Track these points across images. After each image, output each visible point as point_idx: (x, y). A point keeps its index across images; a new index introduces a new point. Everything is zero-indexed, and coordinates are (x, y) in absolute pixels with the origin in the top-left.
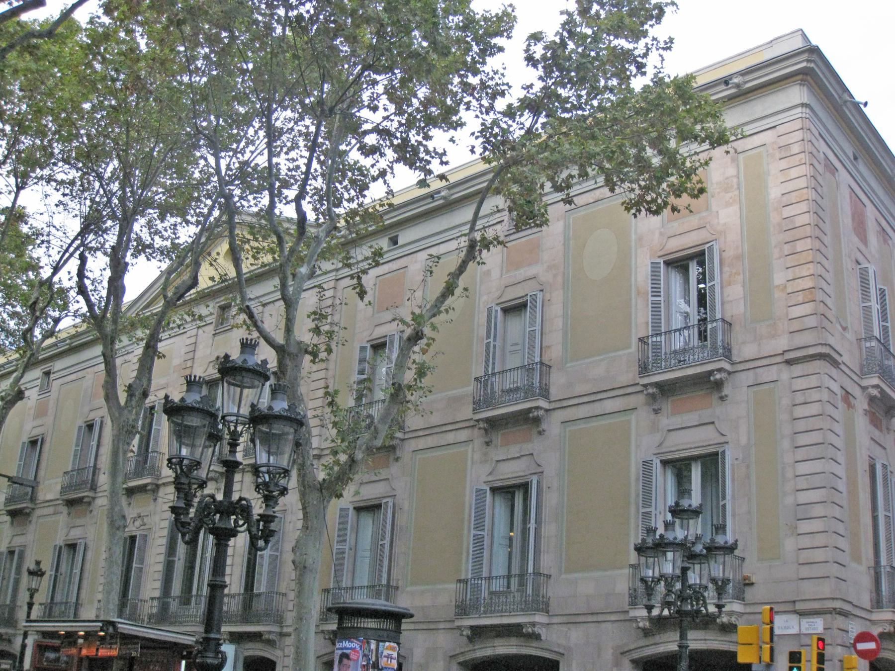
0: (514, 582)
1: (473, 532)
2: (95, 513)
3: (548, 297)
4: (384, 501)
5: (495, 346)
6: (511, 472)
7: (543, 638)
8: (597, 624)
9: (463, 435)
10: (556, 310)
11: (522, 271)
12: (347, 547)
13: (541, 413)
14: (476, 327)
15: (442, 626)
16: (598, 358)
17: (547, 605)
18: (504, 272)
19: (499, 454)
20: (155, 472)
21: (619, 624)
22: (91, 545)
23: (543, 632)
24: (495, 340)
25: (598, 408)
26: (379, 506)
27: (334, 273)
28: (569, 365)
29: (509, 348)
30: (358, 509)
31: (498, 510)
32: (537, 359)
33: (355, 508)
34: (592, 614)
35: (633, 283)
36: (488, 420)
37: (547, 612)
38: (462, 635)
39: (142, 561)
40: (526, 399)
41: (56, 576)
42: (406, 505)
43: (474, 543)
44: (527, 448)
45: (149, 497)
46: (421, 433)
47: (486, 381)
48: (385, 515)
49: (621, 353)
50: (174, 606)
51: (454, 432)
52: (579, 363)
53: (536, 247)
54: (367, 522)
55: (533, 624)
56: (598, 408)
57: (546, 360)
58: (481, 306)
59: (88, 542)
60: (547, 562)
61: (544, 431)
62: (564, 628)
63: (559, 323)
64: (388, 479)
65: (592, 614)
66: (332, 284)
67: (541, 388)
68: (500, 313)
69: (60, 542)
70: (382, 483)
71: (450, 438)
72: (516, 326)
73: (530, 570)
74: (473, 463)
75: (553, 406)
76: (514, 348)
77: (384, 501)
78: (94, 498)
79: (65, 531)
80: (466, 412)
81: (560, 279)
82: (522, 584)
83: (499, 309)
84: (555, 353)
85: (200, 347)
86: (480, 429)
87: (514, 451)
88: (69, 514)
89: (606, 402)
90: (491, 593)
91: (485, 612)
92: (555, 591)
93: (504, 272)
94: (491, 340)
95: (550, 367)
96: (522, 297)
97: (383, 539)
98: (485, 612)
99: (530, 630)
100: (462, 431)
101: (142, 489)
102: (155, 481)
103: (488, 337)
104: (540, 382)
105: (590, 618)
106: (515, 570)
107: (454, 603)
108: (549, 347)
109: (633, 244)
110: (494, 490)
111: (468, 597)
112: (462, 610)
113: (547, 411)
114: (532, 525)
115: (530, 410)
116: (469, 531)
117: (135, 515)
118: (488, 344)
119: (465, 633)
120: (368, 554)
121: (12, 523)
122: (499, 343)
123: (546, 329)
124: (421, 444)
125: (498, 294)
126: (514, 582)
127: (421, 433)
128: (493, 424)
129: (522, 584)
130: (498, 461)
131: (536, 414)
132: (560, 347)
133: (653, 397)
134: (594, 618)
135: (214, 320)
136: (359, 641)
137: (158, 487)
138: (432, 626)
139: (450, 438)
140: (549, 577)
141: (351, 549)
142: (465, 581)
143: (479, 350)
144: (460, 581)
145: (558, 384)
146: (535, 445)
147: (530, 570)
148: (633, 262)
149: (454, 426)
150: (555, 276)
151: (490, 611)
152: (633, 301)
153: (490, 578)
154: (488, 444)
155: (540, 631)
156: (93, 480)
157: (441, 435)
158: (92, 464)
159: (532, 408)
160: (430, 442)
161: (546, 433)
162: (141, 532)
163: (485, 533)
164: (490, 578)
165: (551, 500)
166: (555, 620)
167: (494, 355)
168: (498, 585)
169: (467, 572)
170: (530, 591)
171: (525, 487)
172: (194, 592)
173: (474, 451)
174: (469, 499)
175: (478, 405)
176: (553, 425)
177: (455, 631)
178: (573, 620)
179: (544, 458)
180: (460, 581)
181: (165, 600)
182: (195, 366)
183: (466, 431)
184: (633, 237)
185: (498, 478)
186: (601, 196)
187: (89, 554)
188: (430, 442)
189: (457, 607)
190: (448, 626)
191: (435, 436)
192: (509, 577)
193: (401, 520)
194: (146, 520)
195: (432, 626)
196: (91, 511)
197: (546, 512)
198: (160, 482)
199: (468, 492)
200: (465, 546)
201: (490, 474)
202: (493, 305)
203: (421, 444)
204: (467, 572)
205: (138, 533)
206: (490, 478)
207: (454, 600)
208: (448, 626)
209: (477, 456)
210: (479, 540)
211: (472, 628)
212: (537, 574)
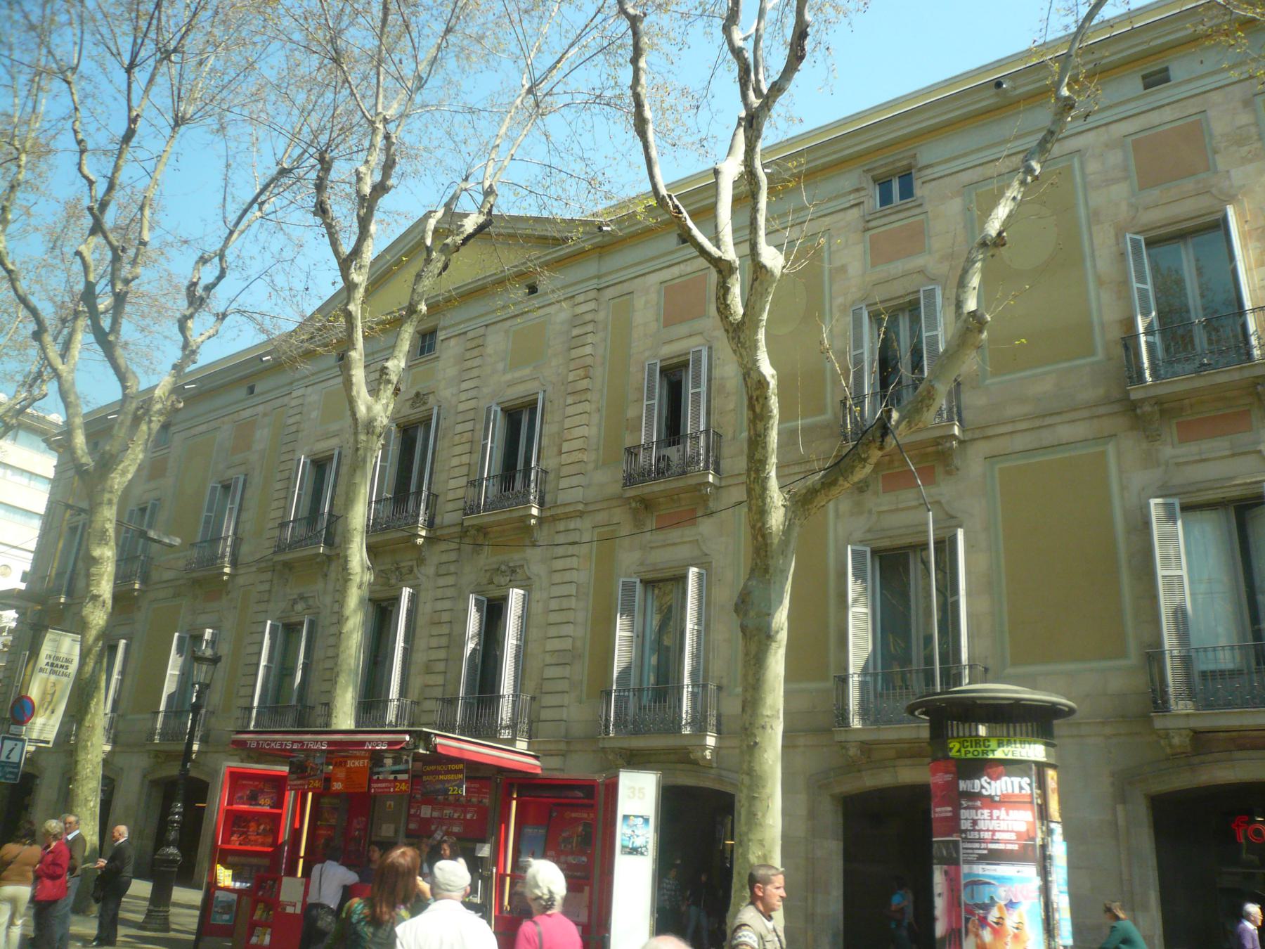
28: (988, 382)
66: (593, 294)
110: (648, 584)
176: (974, 464)
184: (1082, 212)
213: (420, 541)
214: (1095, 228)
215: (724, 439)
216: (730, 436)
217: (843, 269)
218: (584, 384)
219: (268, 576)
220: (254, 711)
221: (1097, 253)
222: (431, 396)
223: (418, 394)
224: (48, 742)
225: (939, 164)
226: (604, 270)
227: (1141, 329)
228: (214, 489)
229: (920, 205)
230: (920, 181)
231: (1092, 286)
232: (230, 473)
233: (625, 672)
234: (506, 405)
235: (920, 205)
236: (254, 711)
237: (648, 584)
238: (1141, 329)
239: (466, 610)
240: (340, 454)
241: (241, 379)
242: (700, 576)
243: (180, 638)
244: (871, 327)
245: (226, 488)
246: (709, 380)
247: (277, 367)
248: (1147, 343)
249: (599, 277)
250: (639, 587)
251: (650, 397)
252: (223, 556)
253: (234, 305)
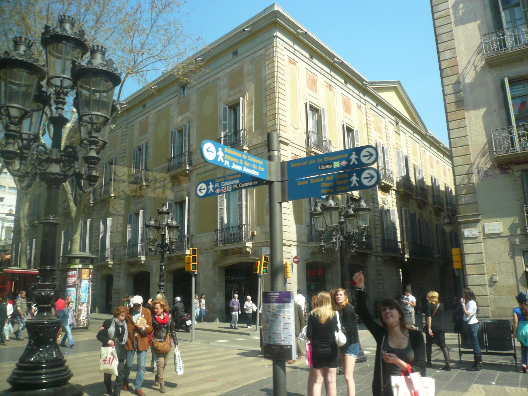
21: (306, 248)
66: (125, 126)
208: (212, 251)
213: (91, 205)
218: (124, 155)
220: (61, 258)
225: (224, 64)
227: (222, 136)
228: (225, 109)
232: (141, 143)
233: (130, 241)
234: (230, 105)
236: (61, 258)
238: (222, 136)
239: (100, 225)
240: (115, 160)
241: (140, 103)
242: (144, 212)
243: (64, 233)
244: (230, 112)
245: (140, 150)
246: (189, 135)
247: (152, 96)
248: (224, 140)
251: (225, 120)
252: (185, 162)
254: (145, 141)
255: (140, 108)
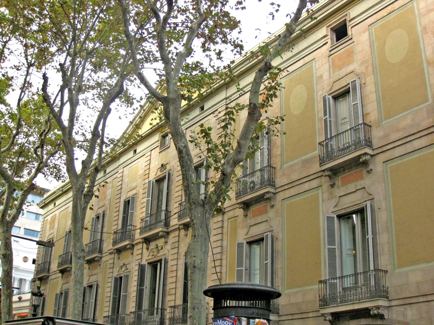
0: (361, 278)
1: (327, 247)
2: (102, 266)
3: (363, 81)
4: (265, 234)
5: (330, 121)
6: (349, 202)
7: (386, 317)
8: (427, 303)
9: (314, 184)
10: (370, 88)
11: (344, 70)
12: (244, 268)
13: (368, 157)
14: (316, 112)
15: (311, 315)
16: (404, 113)
17: (387, 292)
18: (332, 73)
19: (339, 191)
20: (131, 237)
22: (100, 285)
23: (385, 312)
24: (330, 117)
25: (409, 147)
26: (262, 240)
27: (225, 101)
28: (383, 123)
29: (340, 122)
30: (250, 243)
31: (343, 231)
32: (361, 122)
33: (247, 243)
34: (423, 296)
35: (424, 57)
36: (330, 169)
37: (387, 298)
38: (325, 320)
39: (126, 291)
40: (356, 150)
41: (83, 305)
42: (280, 236)
43: (329, 255)
44: (360, 184)
45: (130, 252)
46: (286, 187)
47: (327, 144)
48: (267, 245)
49: (422, 106)
50: (144, 316)
51: (308, 183)
52: (391, 119)
53: (350, 54)
54: (256, 249)
55: (378, 307)
56: (409, 147)
57: (367, 122)
58: (319, 98)
59: (99, 283)
60: (384, 262)
61: (371, 170)
62: (402, 309)
63: (373, 97)
64: (267, 220)
65: (423, 296)
67: (366, 140)
68: (331, 100)
69: (85, 284)
70: (264, 223)
71: (306, 186)
72: (344, 107)
73: (372, 268)
74: (323, 201)
75: (376, 152)
76: (343, 121)
77: (265, 234)
78: (101, 258)
79: (87, 278)
80: (316, 167)
81: (370, 69)
82: (367, 280)
83: (330, 97)
84: (372, 117)
85: (152, 161)
86: (326, 176)
87: (351, 187)
88: (89, 269)
89: (414, 142)
90: (344, 289)
91: (341, 302)
92: (389, 282)
93: (332, 73)
94: (328, 116)
95: (371, 126)
96: (346, 86)
97: (266, 260)
98: (341, 302)
99: (376, 312)
100: (314, 181)
101: (124, 248)
102: (131, 243)
103: (325, 115)
104: (365, 136)
105: (421, 299)
106: (360, 269)
107: (318, 299)
108: (367, 114)
109: (420, 34)
110: (340, 217)
111: (328, 293)
112: (324, 302)
113: (372, 156)
114: (370, 236)
115: (359, 157)
116: (325, 246)
117: (122, 265)
118: (326, 120)
119: (327, 319)
120: (258, 272)
121: (62, 277)
122: (333, 119)
123: (365, 103)
124: (288, 194)
125: (329, 88)
126: (361, 278)
127: (286, 187)
128: (334, 172)
129: (367, 280)
130: (340, 197)
131: (364, 158)
132: (376, 112)
133: (329, 176)
134: (425, 299)
135: (159, 144)
136: (231, 319)
137: (133, 246)
138: (304, 316)
139: (306, 186)
140: (386, 272)
141: (247, 270)
142: (325, 282)
143: (319, 126)
144: (320, 282)
145: (377, 135)
146: (366, 181)
147: (372, 268)
148: (422, 44)
149: (309, 178)
150: (367, 68)
151: (343, 302)
152: (426, 71)
153: (342, 277)
154: (332, 186)
155: (383, 312)
156: (100, 247)
157: (300, 186)
158: (99, 238)
159: (361, 155)
160: (293, 192)
161: (373, 172)
162: (125, 274)
163: (336, 247)
164: (342, 277)
165: (382, 217)
166: (394, 303)
167: (330, 126)
168: (348, 282)
169: (325, 275)
170: (373, 283)
171: (361, 212)
172: (156, 306)
173: (322, 194)
174: (323, 224)
175: (322, 162)
176: (378, 165)
177: (321, 318)
178: (407, 302)
179: (376, 187)
180: (320, 282)
181: (139, 313)
182: (150, 173)
183: (316, 180)
184: (419, 29)
185: (342, 208)
186: (392, 10)
187: (100, 291)
188: (293, 192)
189: (320, 300)
190: (315, 314)
191: (296, 187)
192: (356, 274)
193: (278, 245)
194: (128, 266)
195: (304, 316)
196: (100, 265)
197: (379, 227)
198: (134, 243)
199: (321, 220)
200: (322, 258)
201: (336, 206)
202: (326, 94)
203: (288, 194)
204: (325, 275)
205: (122, 275)
206: (336, 209)
207: (318, 296)
208: (315, 314)
209: (326, 196)
210: (332, 252)
211: (333, 314)
212: (377, 270)
214: (424, 36)
215: (277, 169)
216: (279, 168)
217: (321, 76)
219: (112, 256)
221: (426, 49)
222: (167, 165)
223: (162, 165)
224: (346, 118)
226: (228, 95)
229: (351, 39)
230: (350, 27)
231: (425, 65)
235: (351, 39)
237: (340, 217)
249: (226, 99)
250: (336, 219)
253: (106, 181)
254: (103, 209)
255: (131, 154)
